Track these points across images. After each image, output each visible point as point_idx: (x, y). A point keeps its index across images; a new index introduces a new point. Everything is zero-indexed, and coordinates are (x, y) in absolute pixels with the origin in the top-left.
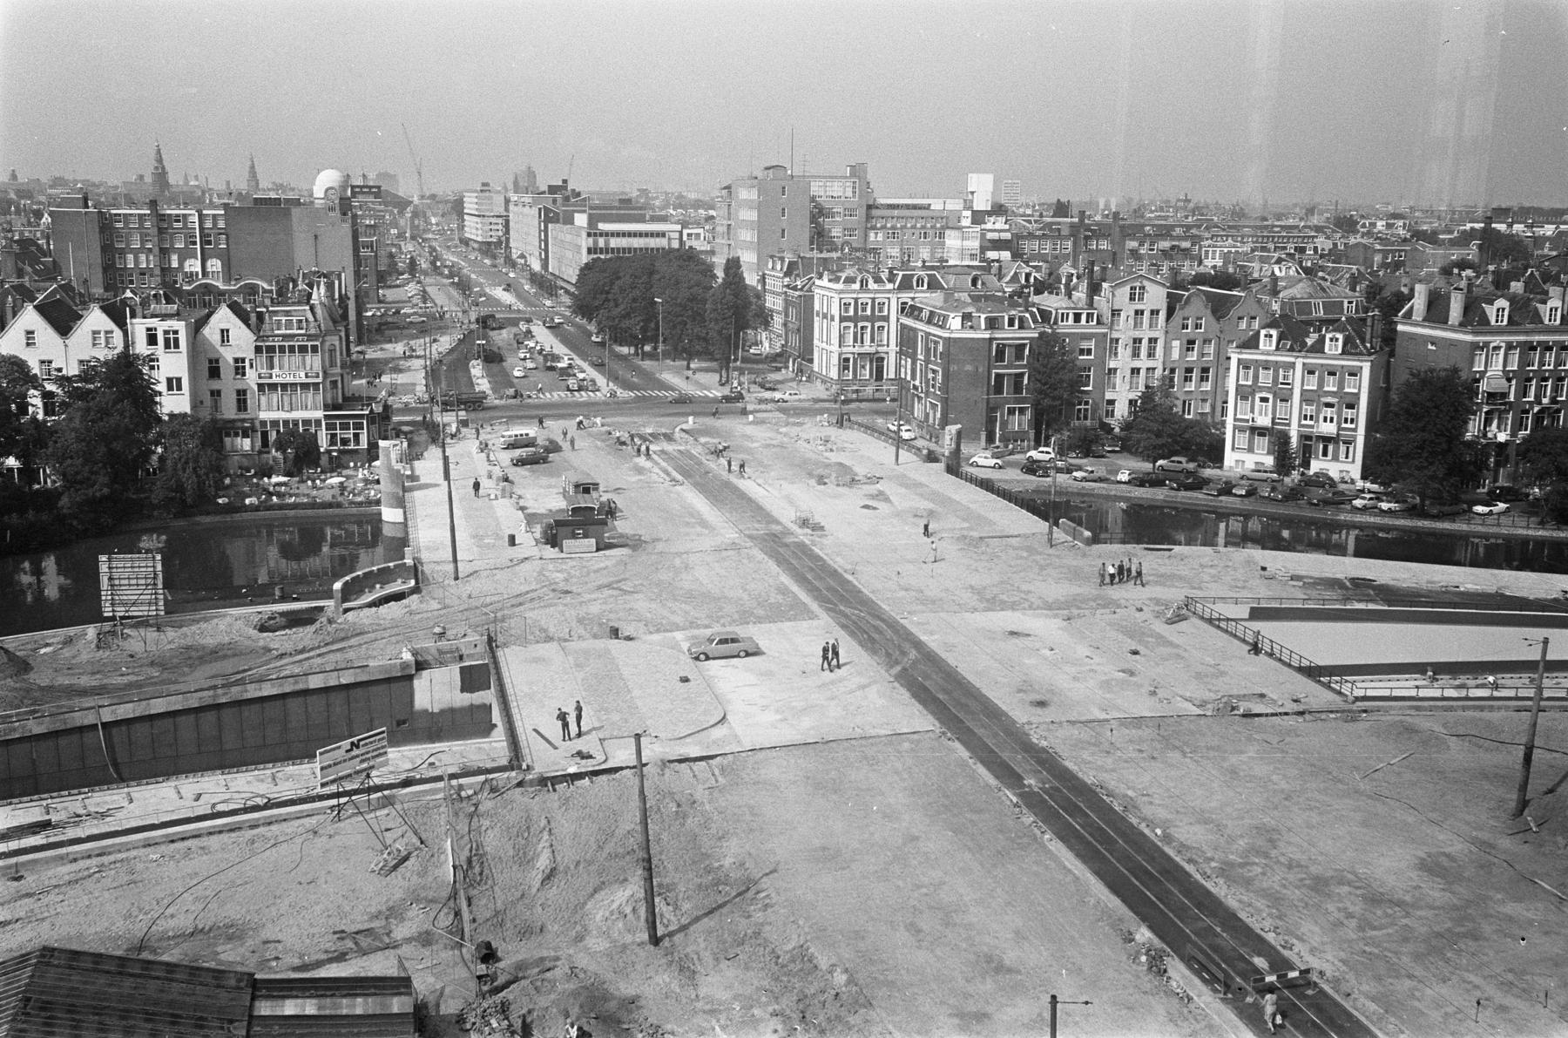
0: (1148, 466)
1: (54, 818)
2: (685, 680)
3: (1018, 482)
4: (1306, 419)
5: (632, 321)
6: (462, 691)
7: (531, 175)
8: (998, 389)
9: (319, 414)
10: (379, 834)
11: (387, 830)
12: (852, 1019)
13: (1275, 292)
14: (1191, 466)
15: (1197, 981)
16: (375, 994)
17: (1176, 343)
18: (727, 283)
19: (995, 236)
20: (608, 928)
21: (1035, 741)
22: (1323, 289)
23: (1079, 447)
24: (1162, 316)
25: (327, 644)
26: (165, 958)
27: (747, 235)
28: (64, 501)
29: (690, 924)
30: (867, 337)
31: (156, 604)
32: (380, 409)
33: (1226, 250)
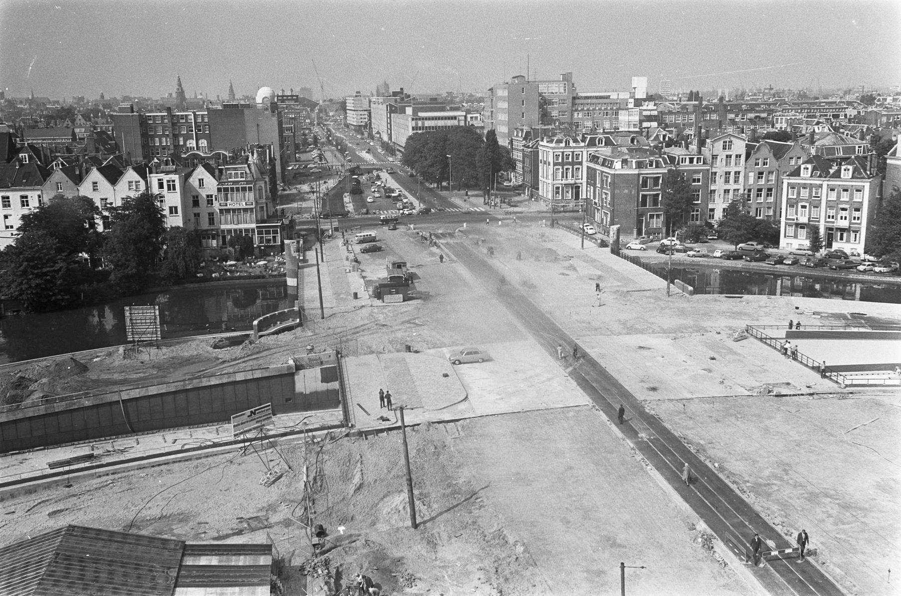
0: (732, 248)
1: (96, 453)
2: (446, 376)
3: (655, 258)
4: (829, 218)
5: (435, 169)
6: (322, 382)
7: (387, 86)
8: (644, 203)
9: (254, 226)
10: (266, 463)
11: (271, 461)
12: (524, 573)
13: (812, 142)
14: (760, 247)
15: (731, 554)
16: (251, 554)
17: (751, 174)
18: (488, 146)
19: (648, 113)
20: (390, 518)
21: (647, 411)
22: (842, 139)
23: (691, 237)
24: (743, 158)
25: (248, 356)
26: (144, 532)
27: (503, 117)
28: (112, 277)
29: (436, 517)
30: (570, 175)
31: (156, 334)
32: (288, 222)
33: (789, 118)
